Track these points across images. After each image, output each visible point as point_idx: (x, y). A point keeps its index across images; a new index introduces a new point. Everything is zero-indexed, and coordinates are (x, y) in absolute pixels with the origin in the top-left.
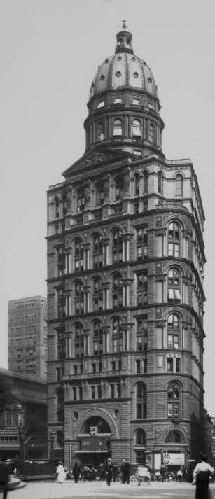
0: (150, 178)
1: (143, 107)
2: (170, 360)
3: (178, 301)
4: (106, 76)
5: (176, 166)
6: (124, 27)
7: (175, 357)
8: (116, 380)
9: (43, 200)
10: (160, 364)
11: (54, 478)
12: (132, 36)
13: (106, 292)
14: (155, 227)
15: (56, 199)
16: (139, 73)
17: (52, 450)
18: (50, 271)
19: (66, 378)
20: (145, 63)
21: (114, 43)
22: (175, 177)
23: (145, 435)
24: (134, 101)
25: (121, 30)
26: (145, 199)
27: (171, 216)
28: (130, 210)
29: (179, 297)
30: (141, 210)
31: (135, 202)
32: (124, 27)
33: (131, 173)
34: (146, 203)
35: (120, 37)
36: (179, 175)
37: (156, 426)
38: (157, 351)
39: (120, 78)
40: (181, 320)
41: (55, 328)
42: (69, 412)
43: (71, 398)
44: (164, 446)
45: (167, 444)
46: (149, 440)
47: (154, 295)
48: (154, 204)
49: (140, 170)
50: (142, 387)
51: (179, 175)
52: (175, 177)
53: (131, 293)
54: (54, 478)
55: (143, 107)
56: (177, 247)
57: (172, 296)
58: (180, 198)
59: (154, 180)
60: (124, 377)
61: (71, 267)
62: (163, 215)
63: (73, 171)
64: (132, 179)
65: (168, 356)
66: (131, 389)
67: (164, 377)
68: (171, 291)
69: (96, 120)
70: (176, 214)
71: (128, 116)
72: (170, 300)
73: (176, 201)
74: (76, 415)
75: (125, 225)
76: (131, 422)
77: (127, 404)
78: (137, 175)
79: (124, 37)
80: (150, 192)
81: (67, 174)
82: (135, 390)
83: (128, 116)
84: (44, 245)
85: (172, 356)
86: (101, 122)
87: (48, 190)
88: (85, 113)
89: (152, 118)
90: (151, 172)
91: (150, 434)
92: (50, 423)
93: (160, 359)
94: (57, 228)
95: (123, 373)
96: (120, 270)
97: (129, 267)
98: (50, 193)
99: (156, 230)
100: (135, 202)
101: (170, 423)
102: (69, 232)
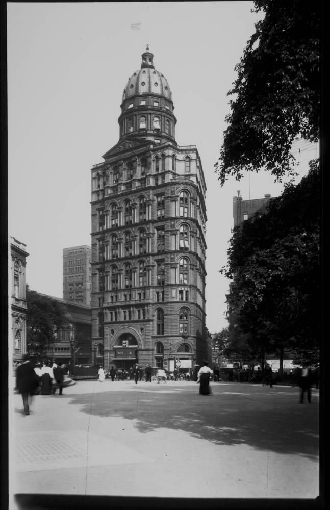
0: (167, 160)
1: (161, 108)
2: (181, 292)
3: (186, 249)
4: (134, 85)
5: (186, 151)
6: (148, 49)
7: (184, 289)
9: (88, 176)
10: (174, 295)
11: (96, 378)
12: (153, 56)
13: (120, 245)
14: (170, 195)
15: (98, 175)
16: (159, 83)
18: (93, 227)
19: (105, 305)
20: (162, 76)
21: (140, 61)
22: (184, 158)
23: (162, 347)
25: (145, 51)
26: (163, 175)
27: (182, 187)
28: (152, 182)
29: (187, 246)
30: (160, 183)
31: (156, 177)
32: (148, 49)
33: (152, 156)
34: (163, 178)
35: (144, 56)
37: (170, 340)
38: (171, 285)
39: (144, 87)
41: (97, 269)
42: (107, 330)
43: (109, 320)
44: (176, 355)
45: (179, 353)
46: (166, 350)
47: (169, 245)
48: (169, 178)
49: (159, 154)
50: (160, 311)
51: (188, 157)
52: (184, 158)
53: (153, 243)
54: (96, 378)
55: (161, 108)
56: (186, 210)
57: (182, 246)
59: (169, 161)
60: (148, 304)
61: (109, 224)
62: (176, 186)
64: (153, 160)
65: (179, 289)
66: (152, 313)
67: (176, 304)
68: (182, 242)
69: (127, 117)
70: (185, 186)
71: (150, 114)
72: (181, 249)
73: (186, 176)
74: (113, 332)
75: (148, 194)
76: (153, 337)
78: (157, 157)
79: (147, 56)
80: (167, 169)
81: (106, 156)
82: (156, 314)
83: (150, 114)
84: (89, 208)
85: (183, 289)
87: (92, 168)
88: (119, 112)
91: (166, 346)
92: (93, 338)
93: (174, 291)
94: (99, 195)
95: (146, 302)
98: (93, 170)
99: (171, 197)
100: (156, 177)
101: (181, 338)
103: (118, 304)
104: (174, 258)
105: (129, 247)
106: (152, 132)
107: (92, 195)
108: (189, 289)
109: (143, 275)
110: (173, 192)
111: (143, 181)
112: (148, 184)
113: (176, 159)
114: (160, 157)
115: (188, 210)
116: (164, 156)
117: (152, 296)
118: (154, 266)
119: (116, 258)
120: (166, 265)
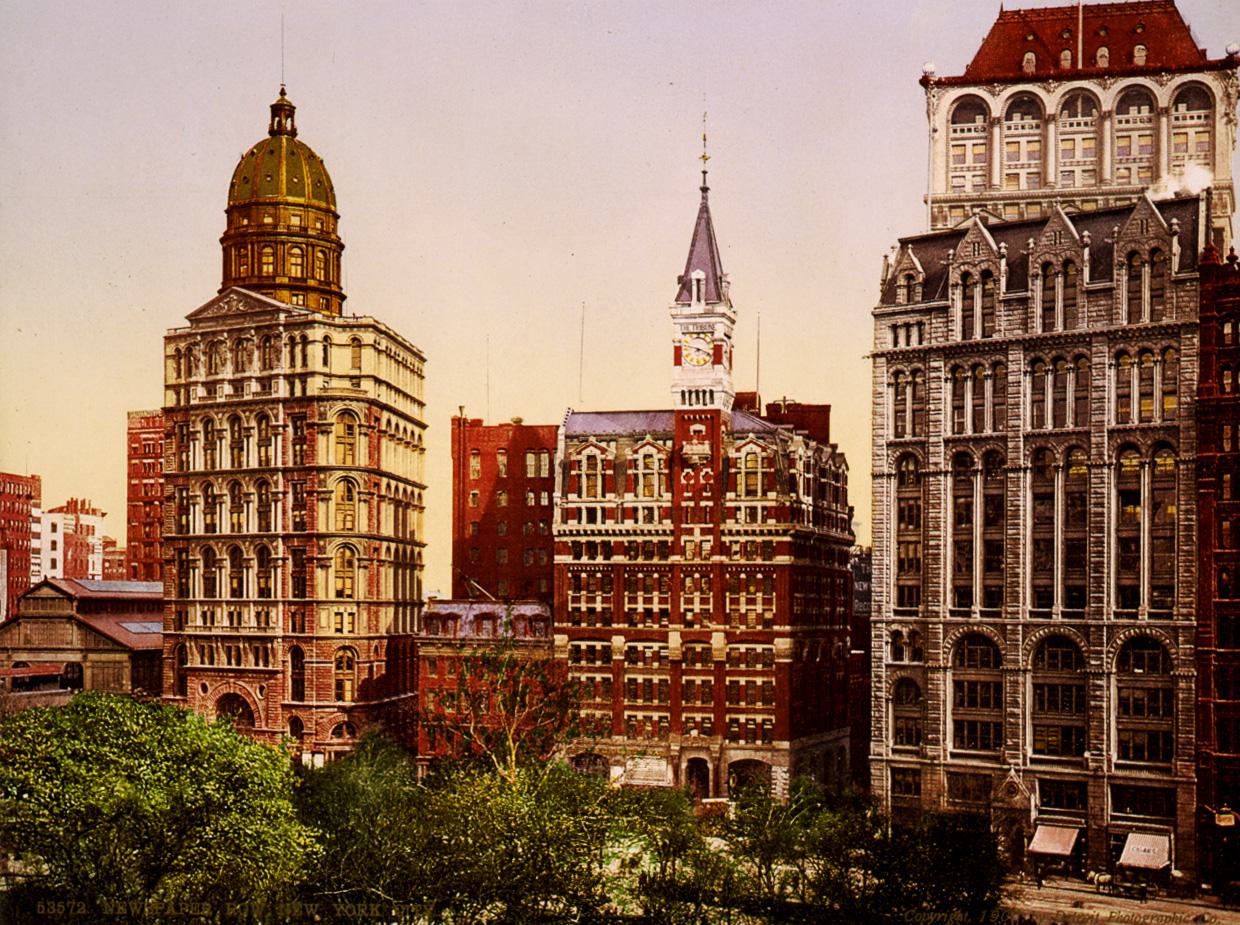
0: (310, 348)
1: (306, 229)
8: (261, 645)
10: (324, 623)
14: (316, 421)
15: (178, 350)
17: (923, 301)
19: (189, 631)
24: (293, 219)
26: (304, 377)
28: (282, 390)
31: (290, 379)
32: (283, 93)
33: (284, 335)
34: (304, 383)
36: (355, 339)
40: (357, 556)
48: (315, 386)
49: (297, 334)
50: (297, 655)
53: (284, 512)
58: (356, 372)
63: (205, 315)
64: (285, 345)
66: (281, 659)
70: (347, 402)
73: (352, 378)
74: (205, 688)
75: (275, 411)
77: (276, 679)
78: (292, 339)
80: (310, 368)
81: (194, 318)
82: (289, 658)
86: (272, 152)
87: (166, 334)
88: (221, 225)
89: (321, 243)
90: (311, 339)
93: (323, 615)
94: (178, 394)
95: (269, 633)
96: (267, 476)
97: (198, 606)
98: (168, 339)
100: (290, 379)
102: (197, 407)
103: (214, 632)
104: (325, 481)
105: (237, 446)
106: (286, 280)
107: (165, 344)
108: (355, 609)
109: (264, 443)
110: (323, 415)
111: (266, 382)
112: (276, 392)
113: (331, 344)
114: (298, 339)
115: (353, 583)
116: (305, 341)
117: (279, 623)
118: (287, 426)
119: (305, 476)
120: (311, 426)
